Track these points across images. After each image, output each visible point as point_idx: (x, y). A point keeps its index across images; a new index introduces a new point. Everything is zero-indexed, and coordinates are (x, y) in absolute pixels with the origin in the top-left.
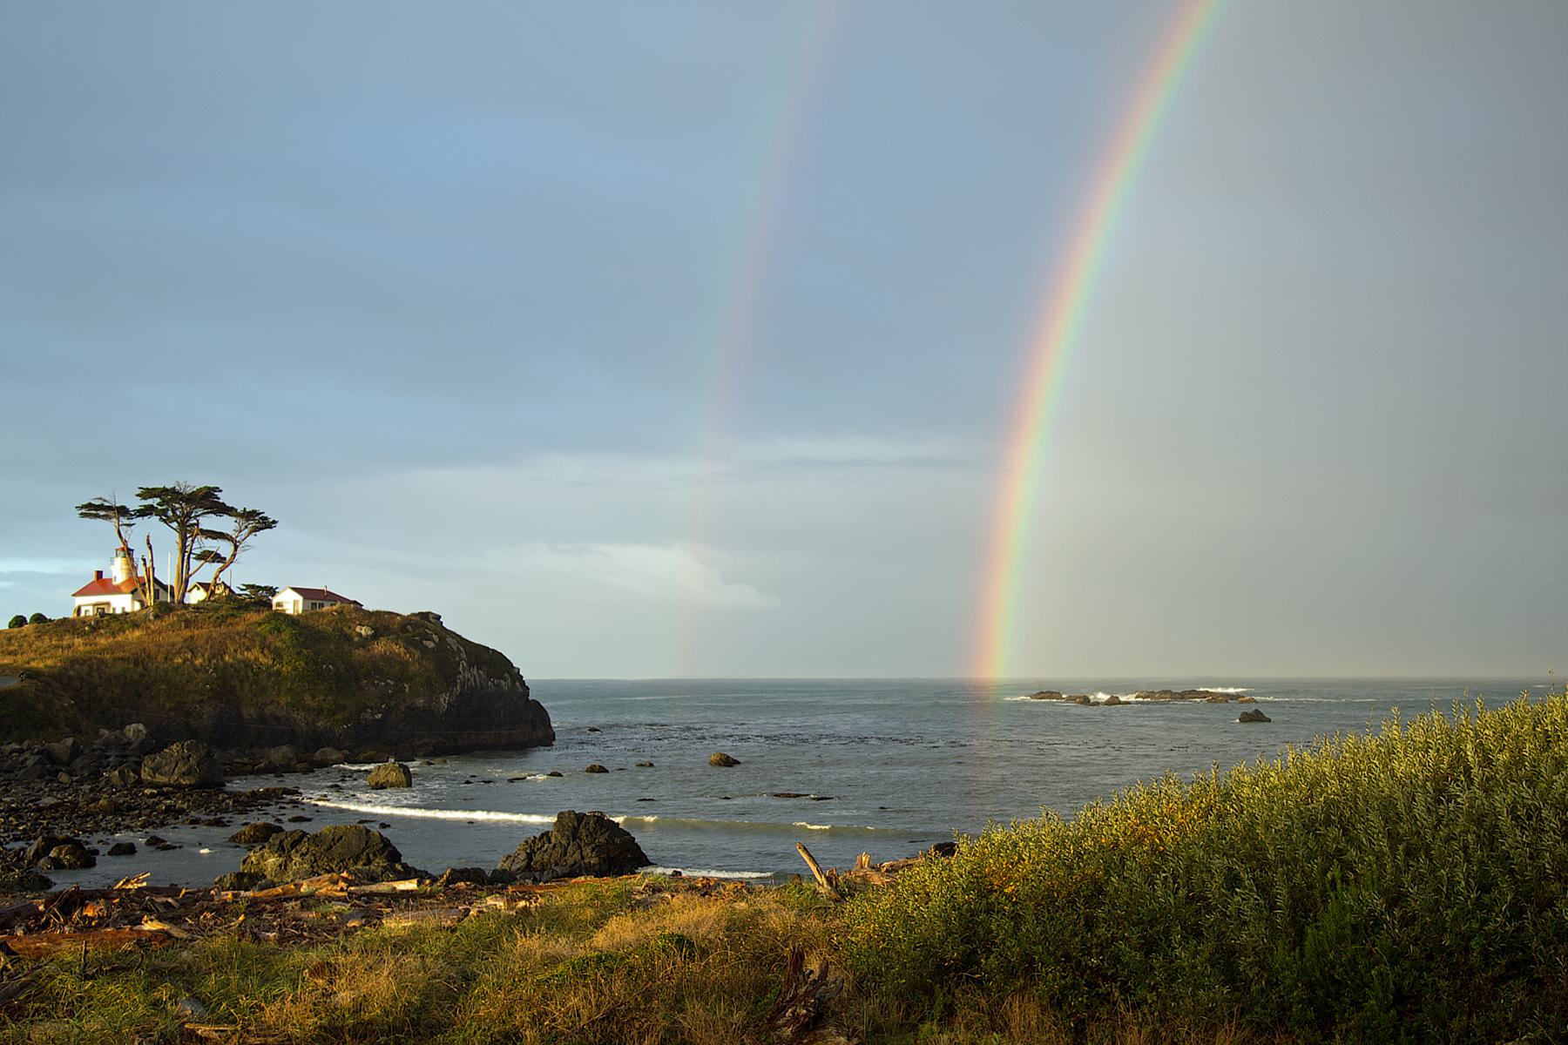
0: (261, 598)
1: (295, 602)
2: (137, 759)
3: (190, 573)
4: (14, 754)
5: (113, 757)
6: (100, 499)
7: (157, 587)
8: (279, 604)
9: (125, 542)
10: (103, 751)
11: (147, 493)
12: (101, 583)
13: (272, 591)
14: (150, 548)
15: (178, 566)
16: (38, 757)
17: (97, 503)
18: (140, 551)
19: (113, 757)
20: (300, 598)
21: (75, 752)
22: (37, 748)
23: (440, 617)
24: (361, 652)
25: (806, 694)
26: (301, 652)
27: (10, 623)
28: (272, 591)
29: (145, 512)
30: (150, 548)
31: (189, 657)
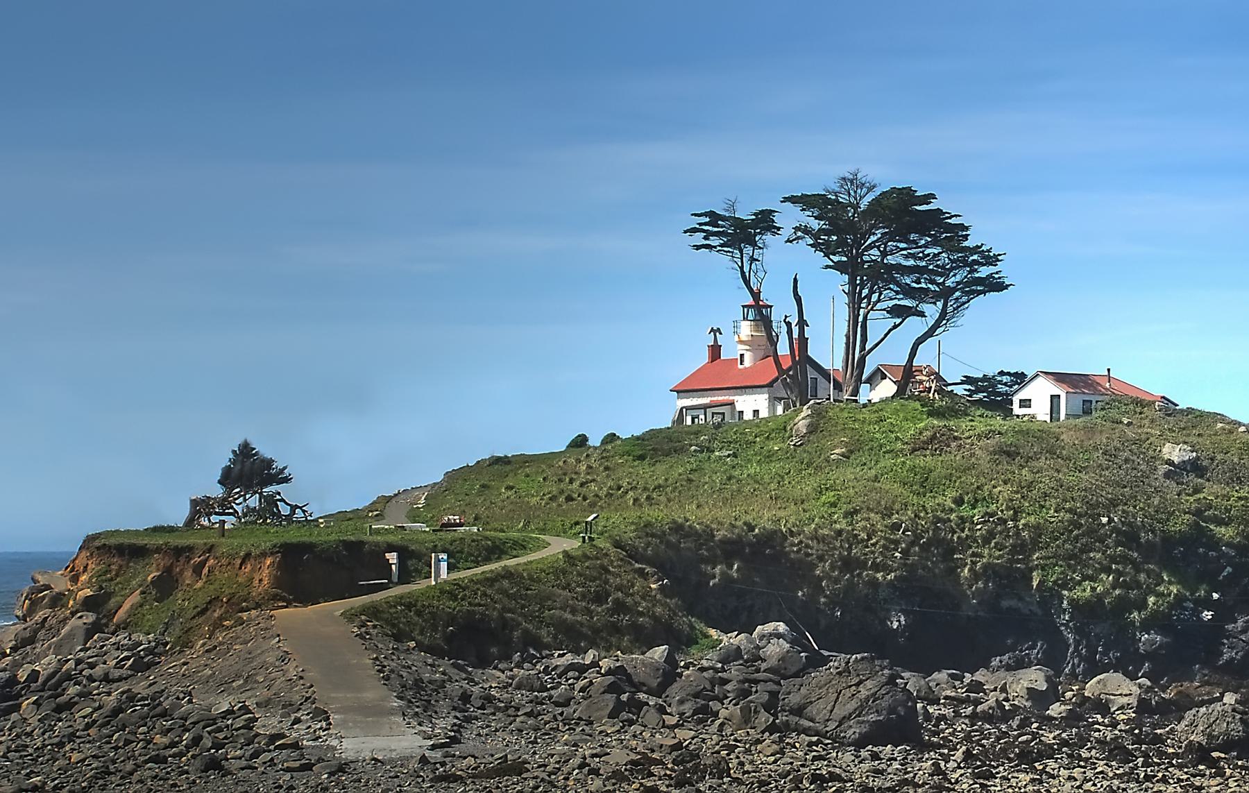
1: (1055, 399)
2: (775, 687)
3: (868, 347)
4: (570, 674)
5: (734, 683)
6: (967, 308)
7: (815, 375)
9: (756, 295)
10: (716, 670)
15: (848, 337)
16: (611, 679)
18: (782, 309)
19: (734, 683)
21: (670, 673)
22: (605, 664)
23: (1002, 371)
24: (450, 772)
26: (269, 687)
27: (602, 441)
31: (240, 580)
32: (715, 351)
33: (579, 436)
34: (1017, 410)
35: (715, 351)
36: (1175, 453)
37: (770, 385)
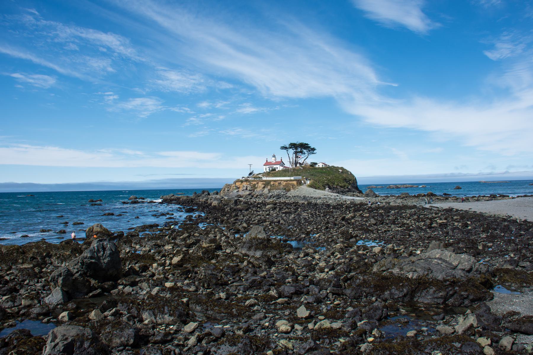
12: (267, 164)
28: (316, 164)
29: (290, 148)
32: (267, 161)
35: (267, 161)
36: (341, 171)
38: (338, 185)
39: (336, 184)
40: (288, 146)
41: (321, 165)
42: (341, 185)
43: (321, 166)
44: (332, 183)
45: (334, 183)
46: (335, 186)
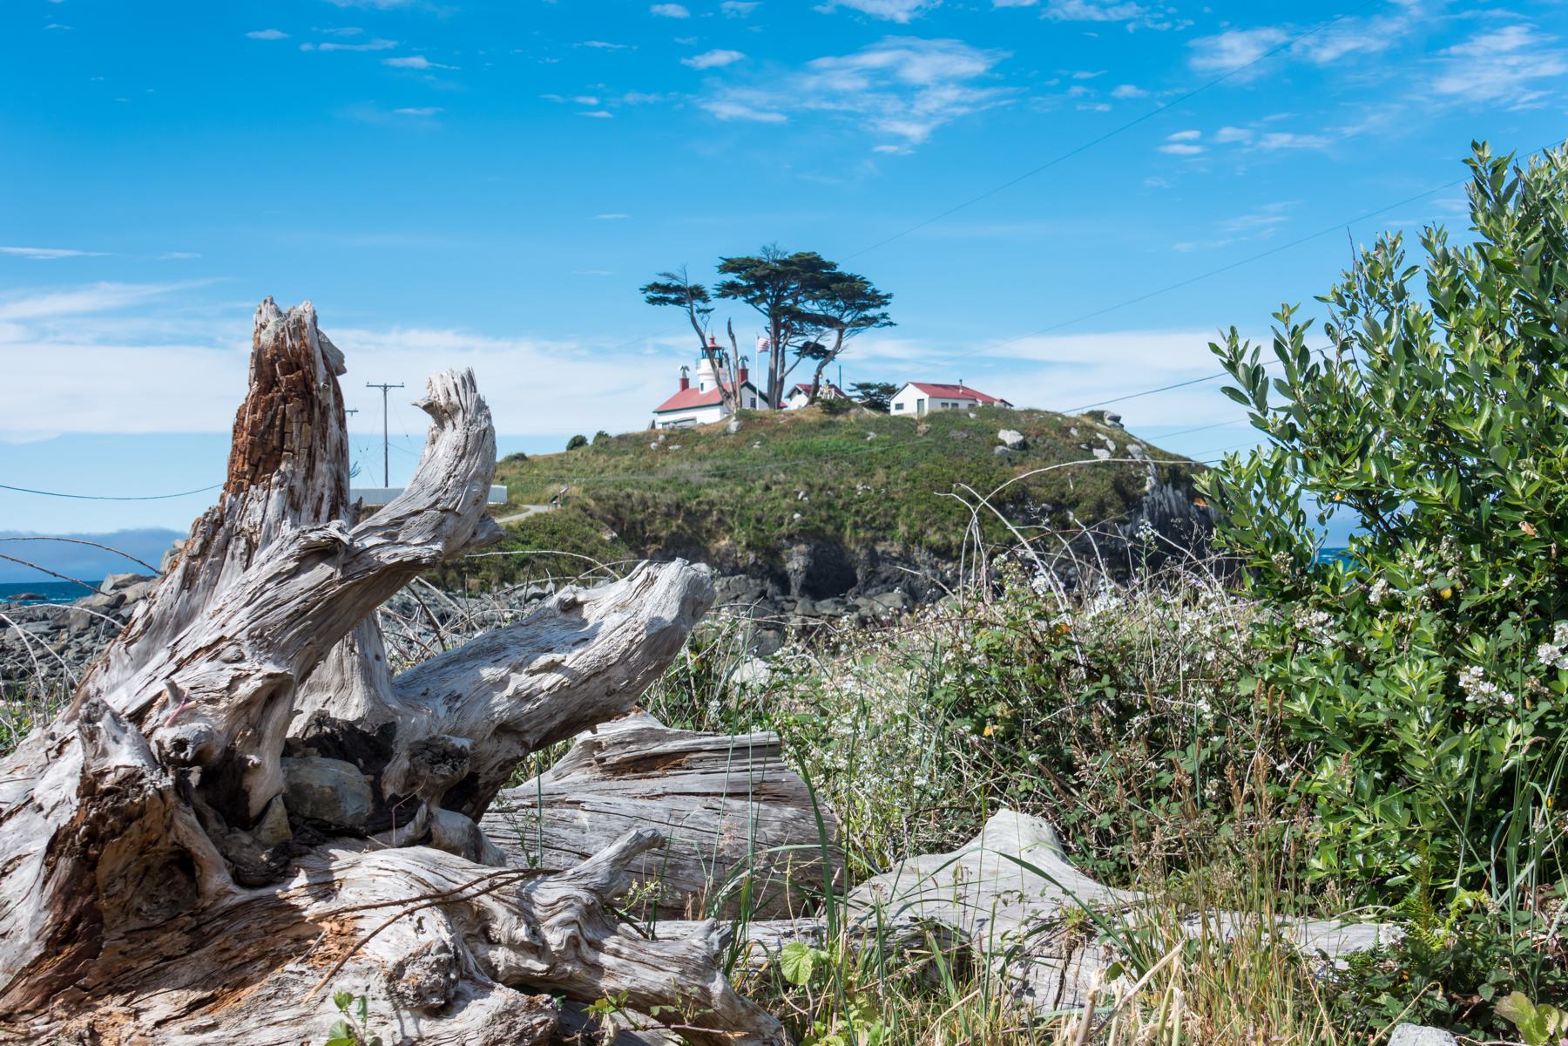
0: (878, 396)
8: (899, 406)
11: (730, 266)
13: (890, 391)
14: (733, 338)
17: (663, 281)
20: (926, 397)
25: (673, 296)
28: (890, 391)
29: (729, 290)
30: (733, 338)
32: (685, 383)
33: (1098, 416)
34: (894, 412)
35: (685, 383)
36: (1010, 437)
37: (721, 404)
38: (915, 538)
39: (902, 529)
40: (710, 280)
41: (909, 403)
42: (934, 537)
43: (910, 410)
44: (868, 525)
45: (890, 526)
46: (896, 549)
